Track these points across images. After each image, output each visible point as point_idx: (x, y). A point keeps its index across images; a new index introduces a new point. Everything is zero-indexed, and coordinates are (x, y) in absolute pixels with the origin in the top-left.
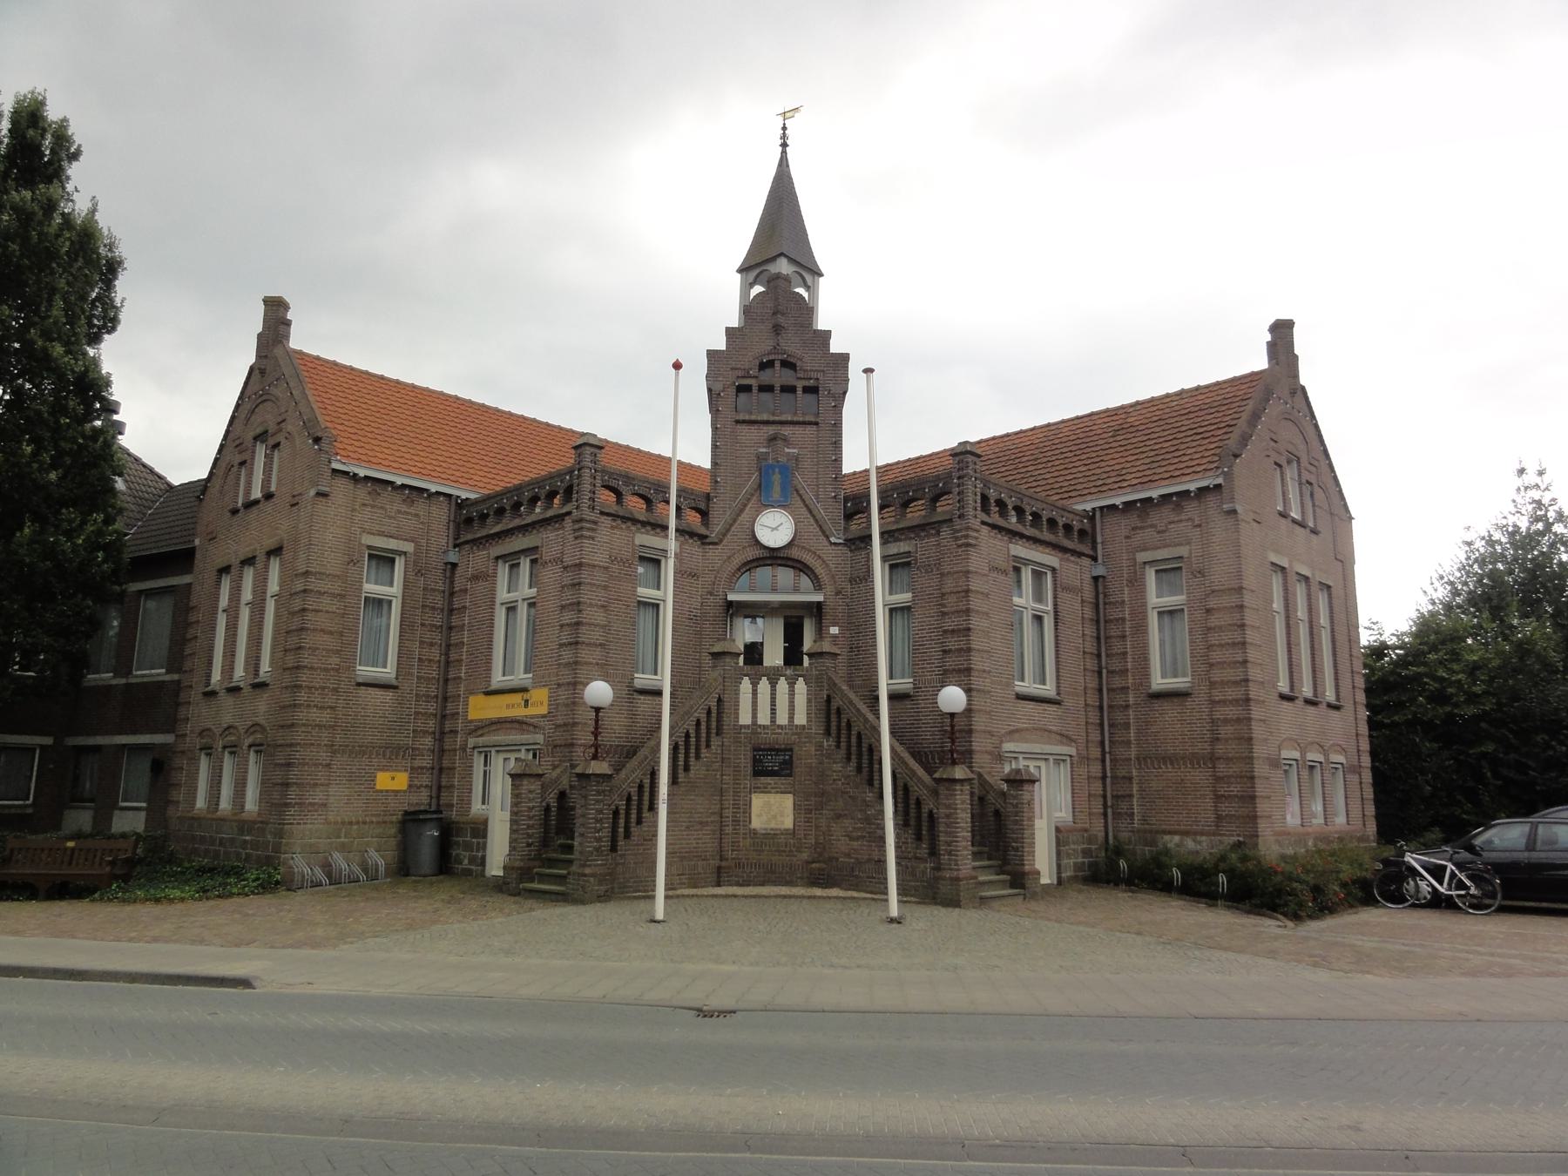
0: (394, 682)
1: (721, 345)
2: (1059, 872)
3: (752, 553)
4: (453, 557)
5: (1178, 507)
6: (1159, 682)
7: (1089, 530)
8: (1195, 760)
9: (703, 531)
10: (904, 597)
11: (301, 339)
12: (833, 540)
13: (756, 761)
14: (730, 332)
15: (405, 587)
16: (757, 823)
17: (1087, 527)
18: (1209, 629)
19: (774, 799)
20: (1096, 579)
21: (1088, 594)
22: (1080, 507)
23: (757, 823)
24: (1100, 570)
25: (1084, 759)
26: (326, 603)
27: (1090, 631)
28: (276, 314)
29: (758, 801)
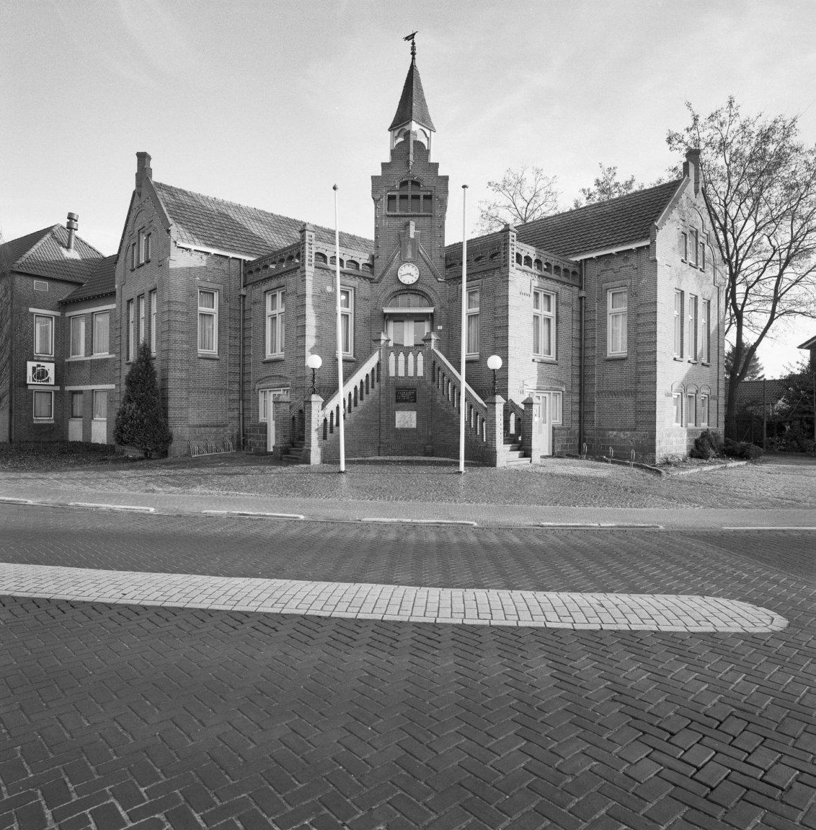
0: (217, 357)
2: (553, 450)
3: (397, 287)
4: (243, 292)
7: (578, 272)
8: (626, 393)
12: (439, 279)
14: (384, 165)
16: (398, 425)
17: (577, 270)
18: (638, 325)
19: (407, 413)
20: (581, 298)
21: (576, 306)
23: (398, 425)
24: (583, 294)
25: (570, 393)
26: (179, 317)
27: (576, 326)
28: (143, 158)
29: (399, 416)
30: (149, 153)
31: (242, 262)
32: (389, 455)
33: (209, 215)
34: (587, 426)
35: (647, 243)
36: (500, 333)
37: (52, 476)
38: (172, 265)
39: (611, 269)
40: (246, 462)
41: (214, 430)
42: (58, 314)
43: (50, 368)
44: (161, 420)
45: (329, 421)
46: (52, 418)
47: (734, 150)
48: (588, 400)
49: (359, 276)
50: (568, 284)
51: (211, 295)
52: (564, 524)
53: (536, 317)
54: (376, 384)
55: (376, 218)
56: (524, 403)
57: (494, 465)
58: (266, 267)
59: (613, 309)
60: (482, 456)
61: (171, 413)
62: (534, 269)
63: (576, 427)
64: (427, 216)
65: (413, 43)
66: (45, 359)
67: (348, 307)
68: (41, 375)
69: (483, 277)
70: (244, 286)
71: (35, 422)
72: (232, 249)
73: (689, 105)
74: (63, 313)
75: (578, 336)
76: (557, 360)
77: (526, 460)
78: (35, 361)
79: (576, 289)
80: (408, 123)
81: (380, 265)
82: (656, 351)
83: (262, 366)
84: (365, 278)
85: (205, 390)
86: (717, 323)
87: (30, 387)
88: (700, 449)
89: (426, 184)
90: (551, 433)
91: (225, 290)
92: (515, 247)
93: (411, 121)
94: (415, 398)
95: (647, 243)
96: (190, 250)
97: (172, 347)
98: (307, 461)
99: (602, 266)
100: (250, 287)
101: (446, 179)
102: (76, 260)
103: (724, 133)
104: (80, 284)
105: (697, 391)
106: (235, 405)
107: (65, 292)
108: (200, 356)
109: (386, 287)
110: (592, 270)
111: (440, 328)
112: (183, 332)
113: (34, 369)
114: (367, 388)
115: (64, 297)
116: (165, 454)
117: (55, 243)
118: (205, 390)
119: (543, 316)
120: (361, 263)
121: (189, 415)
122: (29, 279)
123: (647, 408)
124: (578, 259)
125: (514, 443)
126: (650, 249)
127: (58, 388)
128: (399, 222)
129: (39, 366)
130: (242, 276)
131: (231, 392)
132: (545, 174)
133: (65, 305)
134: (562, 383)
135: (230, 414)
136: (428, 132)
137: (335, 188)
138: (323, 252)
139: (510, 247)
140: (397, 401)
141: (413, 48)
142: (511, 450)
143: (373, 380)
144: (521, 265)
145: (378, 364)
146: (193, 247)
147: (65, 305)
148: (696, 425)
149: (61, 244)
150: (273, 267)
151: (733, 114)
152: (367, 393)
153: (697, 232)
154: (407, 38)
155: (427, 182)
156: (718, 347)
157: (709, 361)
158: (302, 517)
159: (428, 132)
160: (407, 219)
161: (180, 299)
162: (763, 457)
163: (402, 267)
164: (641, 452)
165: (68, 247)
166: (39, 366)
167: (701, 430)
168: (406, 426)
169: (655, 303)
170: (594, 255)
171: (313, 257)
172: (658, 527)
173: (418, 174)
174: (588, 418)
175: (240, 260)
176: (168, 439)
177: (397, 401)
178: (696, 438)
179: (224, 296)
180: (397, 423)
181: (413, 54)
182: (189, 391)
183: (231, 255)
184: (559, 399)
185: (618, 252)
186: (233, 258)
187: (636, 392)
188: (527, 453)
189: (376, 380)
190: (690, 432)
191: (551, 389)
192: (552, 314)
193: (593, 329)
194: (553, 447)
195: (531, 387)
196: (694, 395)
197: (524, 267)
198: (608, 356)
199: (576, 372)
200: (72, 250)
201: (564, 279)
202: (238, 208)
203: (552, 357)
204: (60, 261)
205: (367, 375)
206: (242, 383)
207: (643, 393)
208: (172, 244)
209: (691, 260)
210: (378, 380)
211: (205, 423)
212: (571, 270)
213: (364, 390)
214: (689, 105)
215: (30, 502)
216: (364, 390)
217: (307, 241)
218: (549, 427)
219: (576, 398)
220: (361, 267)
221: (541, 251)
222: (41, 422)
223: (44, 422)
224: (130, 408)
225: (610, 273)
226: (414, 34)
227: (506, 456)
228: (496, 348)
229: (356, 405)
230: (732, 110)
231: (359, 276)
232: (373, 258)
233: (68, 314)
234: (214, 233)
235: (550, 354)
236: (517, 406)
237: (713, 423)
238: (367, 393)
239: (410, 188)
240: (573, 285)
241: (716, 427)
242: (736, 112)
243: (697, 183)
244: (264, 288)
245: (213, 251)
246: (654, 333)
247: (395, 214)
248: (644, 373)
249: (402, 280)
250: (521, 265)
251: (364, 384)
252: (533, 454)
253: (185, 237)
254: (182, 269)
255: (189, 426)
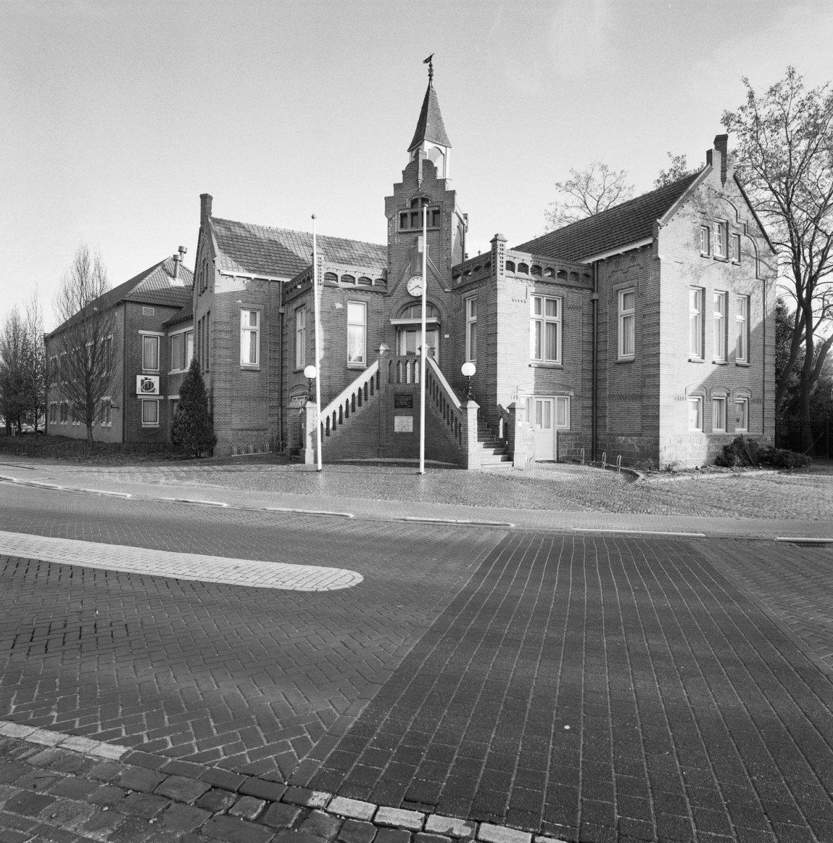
0: (258, 369)
1: (391, 193)
2: (558, 455)
3: (407, 300)
4: (281, 310)
5: (634, 258)
6: (622, 356)
7: (591, 274)
8: (635, 397)
9: (384, 291)
10: (434, 320)
11: (217, 212)
12: (446, 290)
13: (396, 401)
14: (397, 186)
15: (261, 325)
16: (397, 430)
17: (590, 272)
18: (644, 325)
19: (405, 418)
20: (593, 301)
21: (587, 309)
22: (585, 262)
23: (397, 430)
24: (595, 296)
25: (578, 397)
26: (223, 335)
27: (587, 329)
28: (206, 200)
29: (397, 420)
30: (210, 194)
31: (281, 284)
32: (388, 457)
33: (258, 243)
34: (600, 431)
35: (650, 241)
36: (491, 341)
37: (105, 469)
38: (217, 291)
39: (620, 270)
40: (144, 455)
41: (256, 433)
42: (162, 334)
43: (156, 380)
44: (206, 425)
45: (325, 426)
46: (158, 423)
47: (782, 131)
48: (600, 405)
49: (371, 292)
50: (576, 288)
51: (552, 304)
52: (425, 519)
53: (539, 323)
54: (376, 392)
55: (388, 236)
56: (508, 408)
57: (466, 467)
58: (296, 287)
59: (625, 311)
60: (449, 455)
61: (216, 419)
62: (530, 276)
63: (588, 432)
64: (435, 230)
65: (431, 66)
66: (152, 373)
67: (556, 316)
68: (148, 386)
69: (479, 287)
70: (283, 305)
71: (143, 426)
72: (274, 273)
73: (746, 81)
74: (167, 333)
75: (591, 340)
76: (562, 364)
77: (508, 464)
78: (144, 374)
79: (588, 292)
80: (421, 143)
81: (392, 280)
82: (659, 354)
83: (293, 376)
84: (377, 293)
85: (247, 398)
86: (762, 319)
87: (139, 397)
88: (731, 455)
89: (434, 200)
90: (556, 438)
91: (265, 309)
92: (504, 256)
93: (423, 141)
94: (412, 404)
95: (650, 241)
96: (232, 276)
97: (218, 361)
98: (303, 462)
99: (612, 267)
100: (286, 305)
101: (453, 193)
102: (180, 288)
103: (786, 108)
104: (180, 308)
105: (728, 394)
106: (275, 411)
107: (168, 315)
108: (242, 368)
109: (396, 302)
110: (604, 272)
111: (447, 336)
112: (226, 348)
113: (142, 381)
114: (366, 395)
115: (168, 320)
116: (211, 453)
117: (164, 273)
118: (247, 398)
119: (545, 322)
120: (373, 279)
121: (231, 420)
122: (138, 306)
123: (651, 412)
124: (591, 261)
125: (502, 447)
126: (652, 247)
127: (162, 397)
128: (408, 238)
129: (146, 379)
130: (281, 297)
131: (271, 399)
132: (611, 170)
133: (168, 326)
134: (569, 388)
135: (270, 419)
136: (443, 149)
137: (313, 218)
138: (334, 272)
139: (498, 256)
140: (396, 407)
141: (431, 70)
142: (494, 454)
143: (372, 388)
144: (514, 272)
145: (378, 373)
146: (235, 274)
147: (168, 326)
148: (727, 431)
149: (169, 274)
150: (299, 287)
151: (795, 86)
152: (366, 399)
153: (727, 223)
154: (426, 61)
155: (436, 197)
156: (764, 345)
157: (748, 362)
158: (225, 505)
159: (443, 149)
160: (414, 235)
161: (225, 319)
162: (813, 466)
163: (411, 281)
164: (646, 456)
165: (174, 277)
166: (146, 379)
167: (735, 436)
168: (404, 431)
169: (658, 303)
170: (604, 256)
171: (323, 277)
172: (508, 525)
173: (426, 190)
174: (600, 422)
175: (279, 282)
176: (214, 441)
177: (396, 407)
178: (725, 444)
179: (265, 314)
180: (396, 428)
181: (430, 76)
182: (232, 399)
183: (270, 278)
184: (567, 404)
185: (626, 252)
186: (272, 281)
187: (641, 397)
188: (508, 454)
189: (375, 387)
190: (713, 438)
191: (555, 394)
192: (557, 319)
193: (605, 332)
194: (558, 452)
195: (528, 392)
196: (724, 398)
197: (517, 273)
198: (619, 359)
199: (589, 376)
200: (177, 279)
201: (572, 283)
202: (290, 234)
203: (558, 362)
204: (153, 291)
205: (366, 383)
206: (281, 391)
207: (649, 397)
208: (217, 273)
209: (717, 252)
210: (378, 388)
211: (247, 427)
212: (581, 272)
213: (363, 397)
214: (746, 81)
215: (60, 488)
216: (363, 397)
217: (499, 251)
218: (554, 431)
219: (589, 403)
220: (373, 283)
221: (540, 256)
222: (149, 426)
223: (151, 426)
224: (181, 414)
225: (620, 274)
226: (431, 56)
227: (480, 456)
228: (488, 354)
229: (353, 410)
230: (794, 82)
231: (371, 292)
232: (386, 273)
233: (170, 334)
234: (259, 259)
235: (540, 358)
236: (505, 411)
237: (759, 428)
238: (366, 399)
239: (421, 202)
240: (582, 289)
241: (761, 433)
242: (798, 83)
243: (724, 170)
244: (295, 306)
245: (253, 276)
246: (657, 334)
247: (406, 230)
248: (649, 376)
249: (411, 293)
250: (514, 272)
251: (363, 392)
252: (516, 458)
253: (230, 265)
254: (226, 294)
255: (232, 430)
